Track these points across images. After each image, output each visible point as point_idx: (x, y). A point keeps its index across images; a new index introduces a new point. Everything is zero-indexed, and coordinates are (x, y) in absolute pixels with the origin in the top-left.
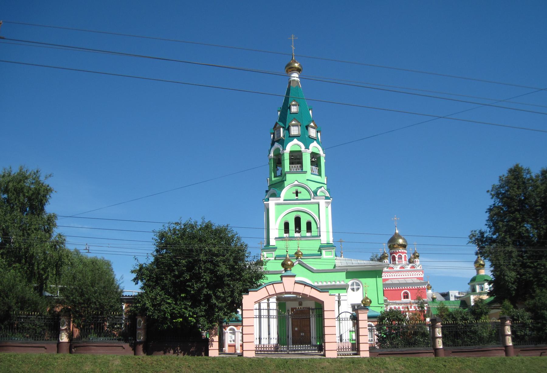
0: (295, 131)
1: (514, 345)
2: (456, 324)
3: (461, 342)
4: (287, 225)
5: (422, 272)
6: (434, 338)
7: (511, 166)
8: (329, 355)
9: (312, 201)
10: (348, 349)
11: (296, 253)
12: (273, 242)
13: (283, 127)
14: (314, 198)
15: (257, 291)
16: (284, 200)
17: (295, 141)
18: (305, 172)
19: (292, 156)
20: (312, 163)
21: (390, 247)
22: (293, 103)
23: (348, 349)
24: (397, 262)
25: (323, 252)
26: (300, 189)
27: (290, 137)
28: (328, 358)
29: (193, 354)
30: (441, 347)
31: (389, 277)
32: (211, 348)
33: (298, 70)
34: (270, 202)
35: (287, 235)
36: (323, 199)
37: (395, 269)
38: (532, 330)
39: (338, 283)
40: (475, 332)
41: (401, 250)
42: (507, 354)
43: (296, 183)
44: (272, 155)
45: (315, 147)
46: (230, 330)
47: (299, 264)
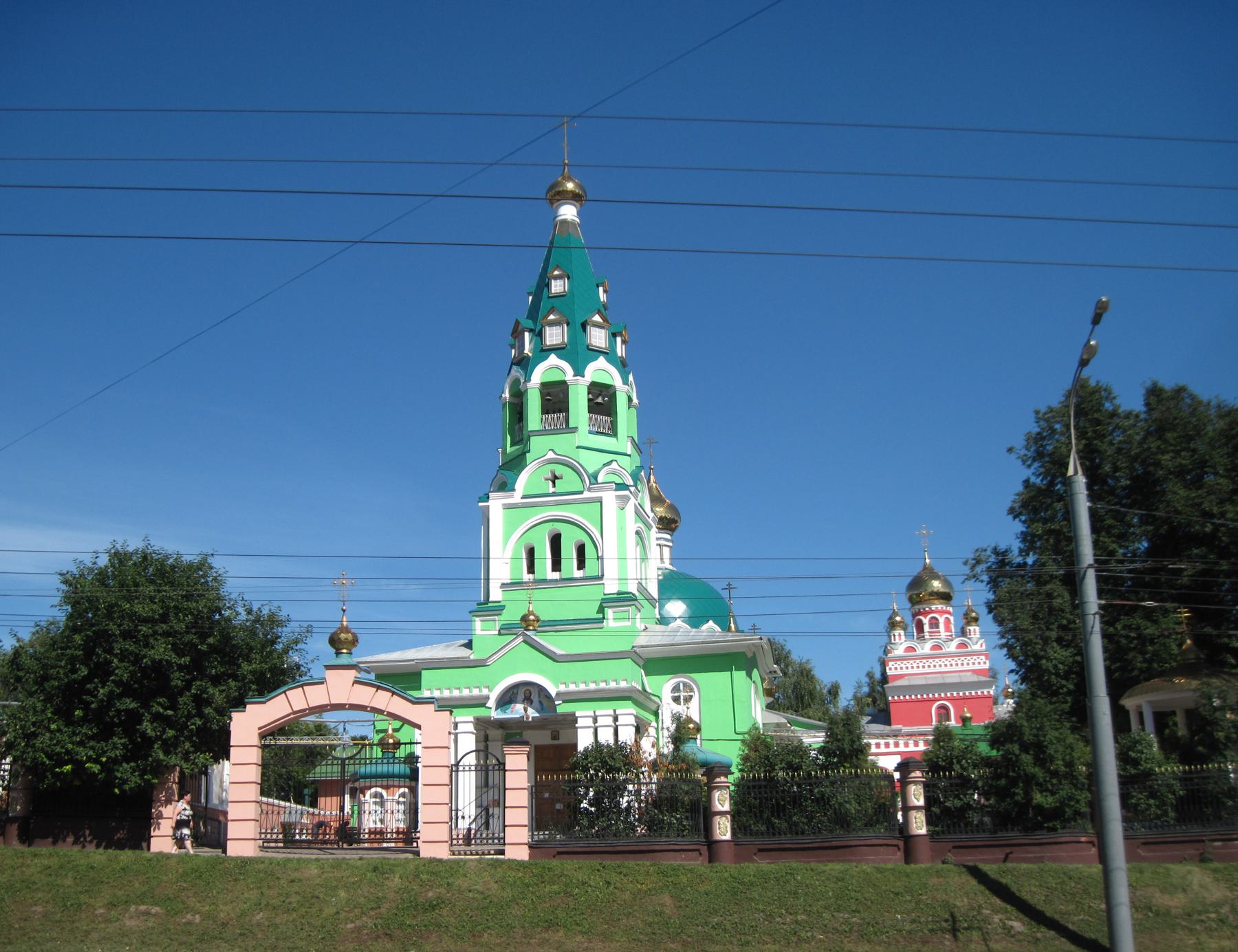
0: (554, 336)
1: (932, 835)
2: (772, 779)
3: (784, 825)
4: (531, 553)
5: (987, 656)
6: (708, 814)
7: (1181, 383)
8: (426, 851)
9: (587, 494)
10: (458, 839)
11: (524, 619)
12: (496, 594)
13: (531, 331)
14: (589, 490)
15: (264, 703)
16: (524, 497)
17: (553, 359)
18: (575, 430)
19: (549, 394)
20: (594, 408)
21: (910, 599)
22: (556, 273)
23: (458, 839)
24: (927, 636)
25: (609, 613)
26: (560, 470)
27: (543, 350)
28: (232, 859)
29: (121, 846)
30: (728, 837)
31: (905, 671)
32: (157, 833)
33: (575, 198)
34: (491, 503)
35: (531, 576)
36: (611, 489)
37: (919, 651)
38: (985, 794)
39: (613, 685)
40: (823, 801)
41: (938, 606)
42: (909, 857)
43: (551, 455)
44: (507, 395)
45: (600, 370)
46: (376, 795)
47: (525, 641)
